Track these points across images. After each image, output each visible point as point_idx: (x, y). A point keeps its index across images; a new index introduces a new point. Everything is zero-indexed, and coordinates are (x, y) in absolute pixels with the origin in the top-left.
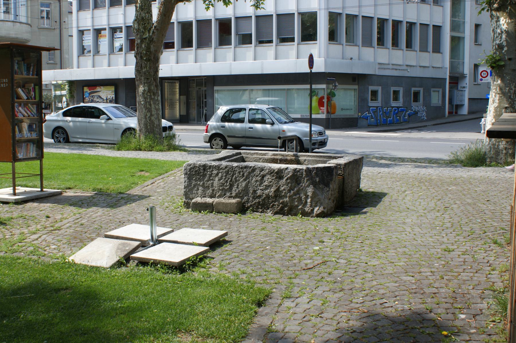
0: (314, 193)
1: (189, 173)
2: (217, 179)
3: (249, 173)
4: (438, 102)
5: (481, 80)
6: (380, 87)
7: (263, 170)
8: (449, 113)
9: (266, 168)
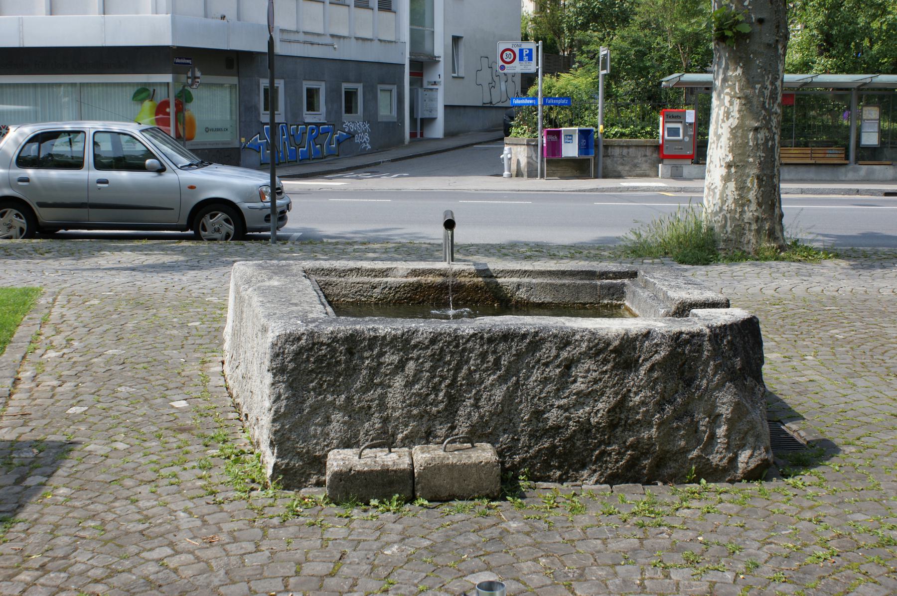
0: (738, 408)
1: (291, 366)
2: (398, 382)
3: (519, 355)
4: (391, 112)
5: (502, 68)
6: (323, 84)
7: (568, 343)
8: (413, 135)
9: (577, 337)
